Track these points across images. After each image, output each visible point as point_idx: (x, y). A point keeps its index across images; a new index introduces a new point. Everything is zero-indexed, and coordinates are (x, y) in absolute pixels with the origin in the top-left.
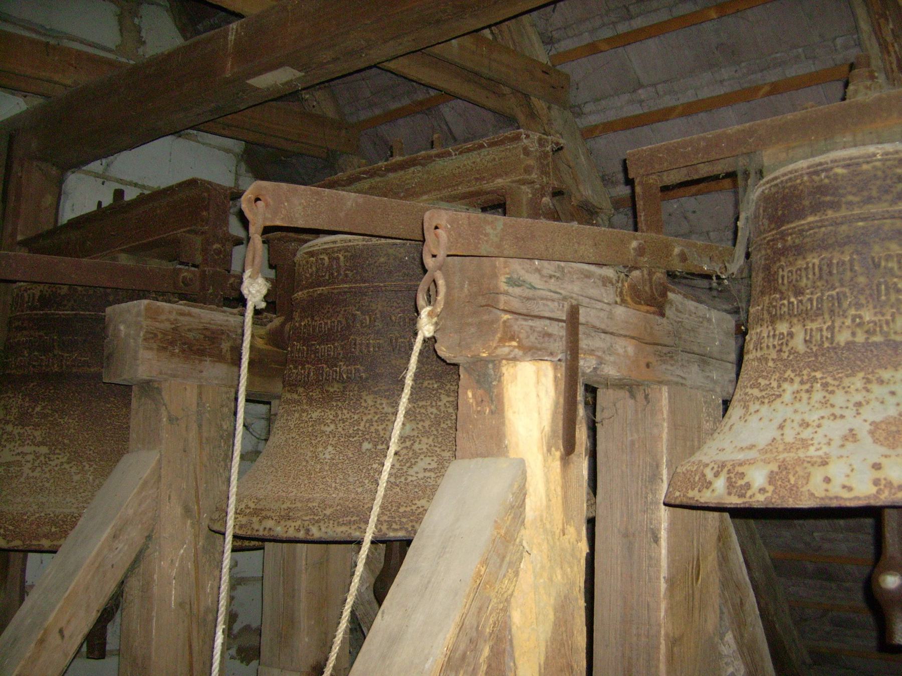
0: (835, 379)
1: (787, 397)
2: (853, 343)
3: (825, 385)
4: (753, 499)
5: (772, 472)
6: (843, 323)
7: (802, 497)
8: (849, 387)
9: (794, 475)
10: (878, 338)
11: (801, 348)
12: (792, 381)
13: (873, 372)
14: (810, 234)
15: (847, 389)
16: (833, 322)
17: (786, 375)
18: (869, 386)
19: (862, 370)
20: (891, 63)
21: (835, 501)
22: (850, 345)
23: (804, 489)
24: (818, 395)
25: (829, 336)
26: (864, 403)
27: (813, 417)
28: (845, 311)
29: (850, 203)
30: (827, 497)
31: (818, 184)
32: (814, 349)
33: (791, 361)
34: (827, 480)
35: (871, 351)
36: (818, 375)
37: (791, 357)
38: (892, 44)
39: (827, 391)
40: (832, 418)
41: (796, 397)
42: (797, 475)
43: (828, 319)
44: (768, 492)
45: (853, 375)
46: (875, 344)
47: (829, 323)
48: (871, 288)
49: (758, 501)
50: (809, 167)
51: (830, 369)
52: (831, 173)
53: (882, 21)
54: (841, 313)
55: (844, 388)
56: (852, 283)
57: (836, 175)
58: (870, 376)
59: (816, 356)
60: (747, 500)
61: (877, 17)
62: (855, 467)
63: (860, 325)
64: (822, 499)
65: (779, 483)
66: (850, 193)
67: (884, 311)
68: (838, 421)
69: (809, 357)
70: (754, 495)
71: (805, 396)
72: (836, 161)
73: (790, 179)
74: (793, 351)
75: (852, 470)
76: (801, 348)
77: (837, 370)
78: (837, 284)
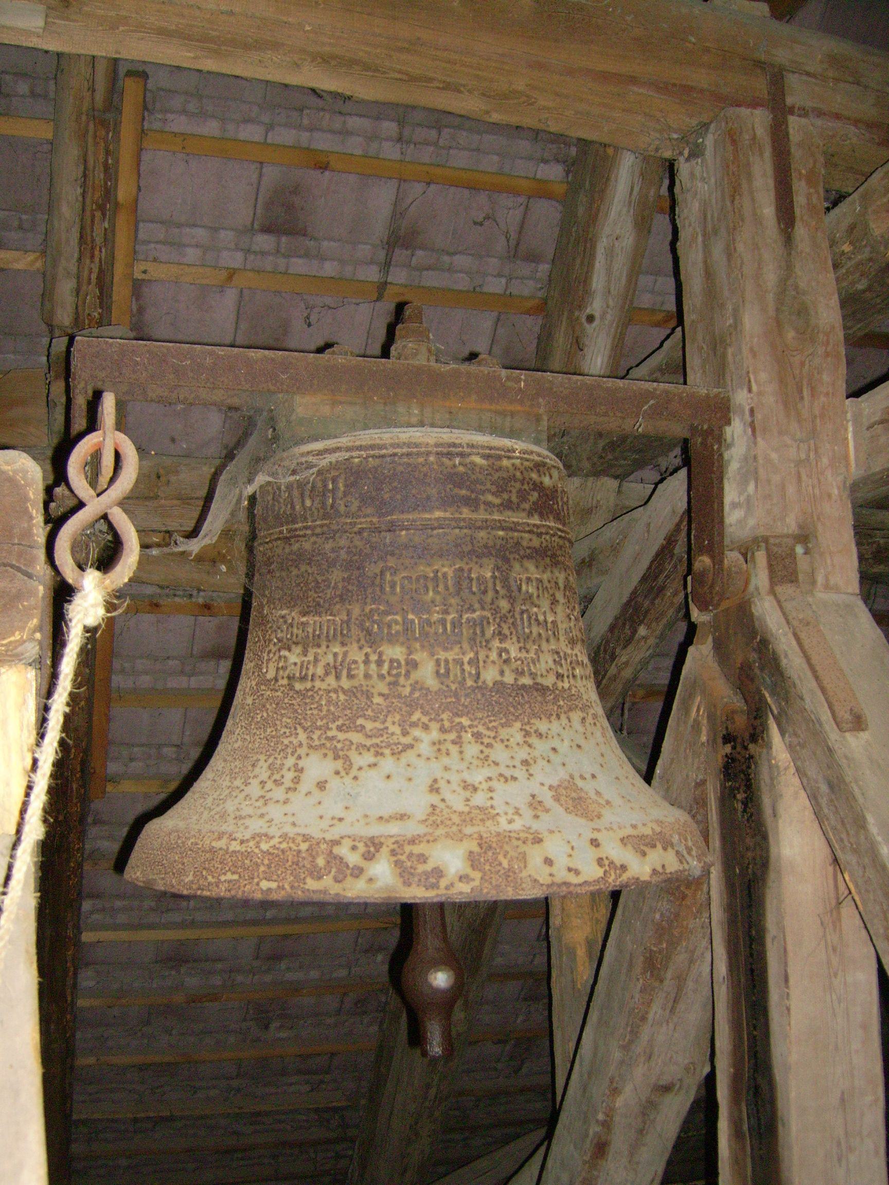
0: (488, 729)
1: (424, 748)
2: (502, 683)
3: (477, 736)
4: (454, 891)
5: (471, 852)
6: (487, 657)
7: (524, 885)
8: (508, 740)
9: (505, 856)
10: (526, 681)
11: (432, 683)
12: (426, 727)
13: (529, 723)
14: (438, 535)
15: (506, 743)
16: (477, 653)
17: (414, 718)
18: (530, 740)
19: (517, 718)
20: (91, 272)
21: (564, 888)
22: (499, 686)
23: (524, 874)
24: (472, 749)
25: (474, 672)
26: (531, 762)
27: (478, 777)
28: (487, 641)
29: (488, 504)
30: (553, 884)
31: (449, 470)
32: (453, 687)
33: (418, 699)
34: (549, 862)
35: (522, 695)
36: (465, 721)
37: (417, 694)
38: (100, 248)
39: (482, 743)
40: (502, 779)
41: (439, 750)
42: (509, 856)
43: (469, 650)
44: (473, 880)
45: (507, 725)
46: (524, 687)
47: (472, 655)
48: (513, 616)
49: (461, 893)
50: (437, 445)
51: (480, 715)
52: (468, 460)
53: (98, 214)
54: (484, 644)
55: (502, 741)
56: (494, 607)
57: (474, 464)
58: (527, 728)
59: (456, 695)
60: (442, 891)
61: (94, 207)
62: (574, 844)
63: (506, 661)
64: (549, 886)
65: (487, 867)
66: (489, 491)
67: (528, 646)
68: (512, 784)
69: (446, 697)
70: (452, 885)
71: (454, 749)
72: (473, 446)
73: (408, 455)
74: (418, 686)
75: (573, 848)
76: (432, 683)
77: (488, 716)
78: (477, 606)
